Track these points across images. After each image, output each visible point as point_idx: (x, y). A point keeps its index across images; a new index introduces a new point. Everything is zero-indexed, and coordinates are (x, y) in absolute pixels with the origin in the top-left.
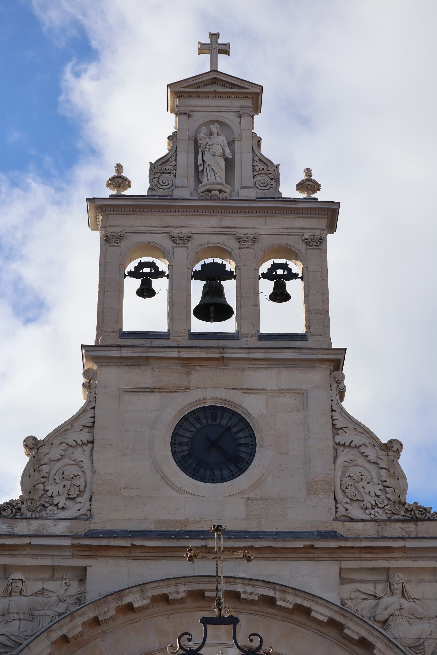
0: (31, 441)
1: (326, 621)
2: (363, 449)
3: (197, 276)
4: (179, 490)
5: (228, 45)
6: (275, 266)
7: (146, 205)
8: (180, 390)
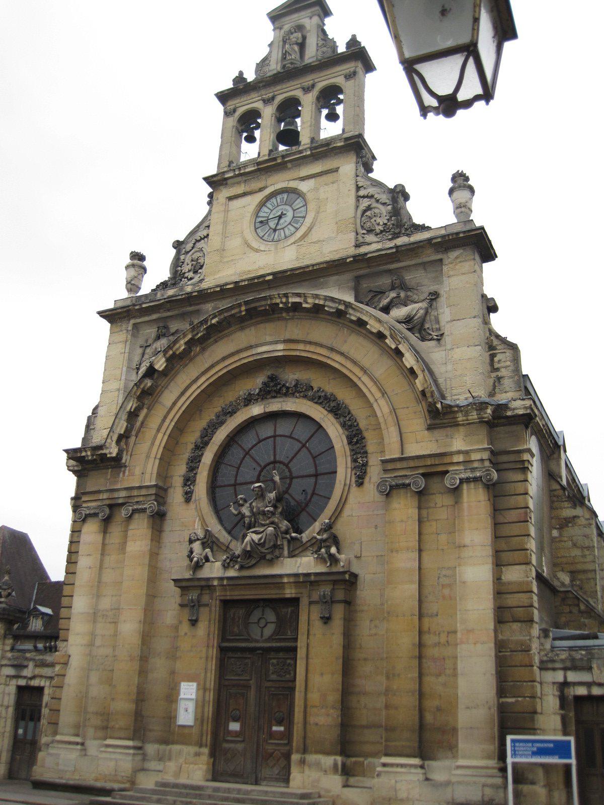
4: (257, 251)
8: (261, 190)
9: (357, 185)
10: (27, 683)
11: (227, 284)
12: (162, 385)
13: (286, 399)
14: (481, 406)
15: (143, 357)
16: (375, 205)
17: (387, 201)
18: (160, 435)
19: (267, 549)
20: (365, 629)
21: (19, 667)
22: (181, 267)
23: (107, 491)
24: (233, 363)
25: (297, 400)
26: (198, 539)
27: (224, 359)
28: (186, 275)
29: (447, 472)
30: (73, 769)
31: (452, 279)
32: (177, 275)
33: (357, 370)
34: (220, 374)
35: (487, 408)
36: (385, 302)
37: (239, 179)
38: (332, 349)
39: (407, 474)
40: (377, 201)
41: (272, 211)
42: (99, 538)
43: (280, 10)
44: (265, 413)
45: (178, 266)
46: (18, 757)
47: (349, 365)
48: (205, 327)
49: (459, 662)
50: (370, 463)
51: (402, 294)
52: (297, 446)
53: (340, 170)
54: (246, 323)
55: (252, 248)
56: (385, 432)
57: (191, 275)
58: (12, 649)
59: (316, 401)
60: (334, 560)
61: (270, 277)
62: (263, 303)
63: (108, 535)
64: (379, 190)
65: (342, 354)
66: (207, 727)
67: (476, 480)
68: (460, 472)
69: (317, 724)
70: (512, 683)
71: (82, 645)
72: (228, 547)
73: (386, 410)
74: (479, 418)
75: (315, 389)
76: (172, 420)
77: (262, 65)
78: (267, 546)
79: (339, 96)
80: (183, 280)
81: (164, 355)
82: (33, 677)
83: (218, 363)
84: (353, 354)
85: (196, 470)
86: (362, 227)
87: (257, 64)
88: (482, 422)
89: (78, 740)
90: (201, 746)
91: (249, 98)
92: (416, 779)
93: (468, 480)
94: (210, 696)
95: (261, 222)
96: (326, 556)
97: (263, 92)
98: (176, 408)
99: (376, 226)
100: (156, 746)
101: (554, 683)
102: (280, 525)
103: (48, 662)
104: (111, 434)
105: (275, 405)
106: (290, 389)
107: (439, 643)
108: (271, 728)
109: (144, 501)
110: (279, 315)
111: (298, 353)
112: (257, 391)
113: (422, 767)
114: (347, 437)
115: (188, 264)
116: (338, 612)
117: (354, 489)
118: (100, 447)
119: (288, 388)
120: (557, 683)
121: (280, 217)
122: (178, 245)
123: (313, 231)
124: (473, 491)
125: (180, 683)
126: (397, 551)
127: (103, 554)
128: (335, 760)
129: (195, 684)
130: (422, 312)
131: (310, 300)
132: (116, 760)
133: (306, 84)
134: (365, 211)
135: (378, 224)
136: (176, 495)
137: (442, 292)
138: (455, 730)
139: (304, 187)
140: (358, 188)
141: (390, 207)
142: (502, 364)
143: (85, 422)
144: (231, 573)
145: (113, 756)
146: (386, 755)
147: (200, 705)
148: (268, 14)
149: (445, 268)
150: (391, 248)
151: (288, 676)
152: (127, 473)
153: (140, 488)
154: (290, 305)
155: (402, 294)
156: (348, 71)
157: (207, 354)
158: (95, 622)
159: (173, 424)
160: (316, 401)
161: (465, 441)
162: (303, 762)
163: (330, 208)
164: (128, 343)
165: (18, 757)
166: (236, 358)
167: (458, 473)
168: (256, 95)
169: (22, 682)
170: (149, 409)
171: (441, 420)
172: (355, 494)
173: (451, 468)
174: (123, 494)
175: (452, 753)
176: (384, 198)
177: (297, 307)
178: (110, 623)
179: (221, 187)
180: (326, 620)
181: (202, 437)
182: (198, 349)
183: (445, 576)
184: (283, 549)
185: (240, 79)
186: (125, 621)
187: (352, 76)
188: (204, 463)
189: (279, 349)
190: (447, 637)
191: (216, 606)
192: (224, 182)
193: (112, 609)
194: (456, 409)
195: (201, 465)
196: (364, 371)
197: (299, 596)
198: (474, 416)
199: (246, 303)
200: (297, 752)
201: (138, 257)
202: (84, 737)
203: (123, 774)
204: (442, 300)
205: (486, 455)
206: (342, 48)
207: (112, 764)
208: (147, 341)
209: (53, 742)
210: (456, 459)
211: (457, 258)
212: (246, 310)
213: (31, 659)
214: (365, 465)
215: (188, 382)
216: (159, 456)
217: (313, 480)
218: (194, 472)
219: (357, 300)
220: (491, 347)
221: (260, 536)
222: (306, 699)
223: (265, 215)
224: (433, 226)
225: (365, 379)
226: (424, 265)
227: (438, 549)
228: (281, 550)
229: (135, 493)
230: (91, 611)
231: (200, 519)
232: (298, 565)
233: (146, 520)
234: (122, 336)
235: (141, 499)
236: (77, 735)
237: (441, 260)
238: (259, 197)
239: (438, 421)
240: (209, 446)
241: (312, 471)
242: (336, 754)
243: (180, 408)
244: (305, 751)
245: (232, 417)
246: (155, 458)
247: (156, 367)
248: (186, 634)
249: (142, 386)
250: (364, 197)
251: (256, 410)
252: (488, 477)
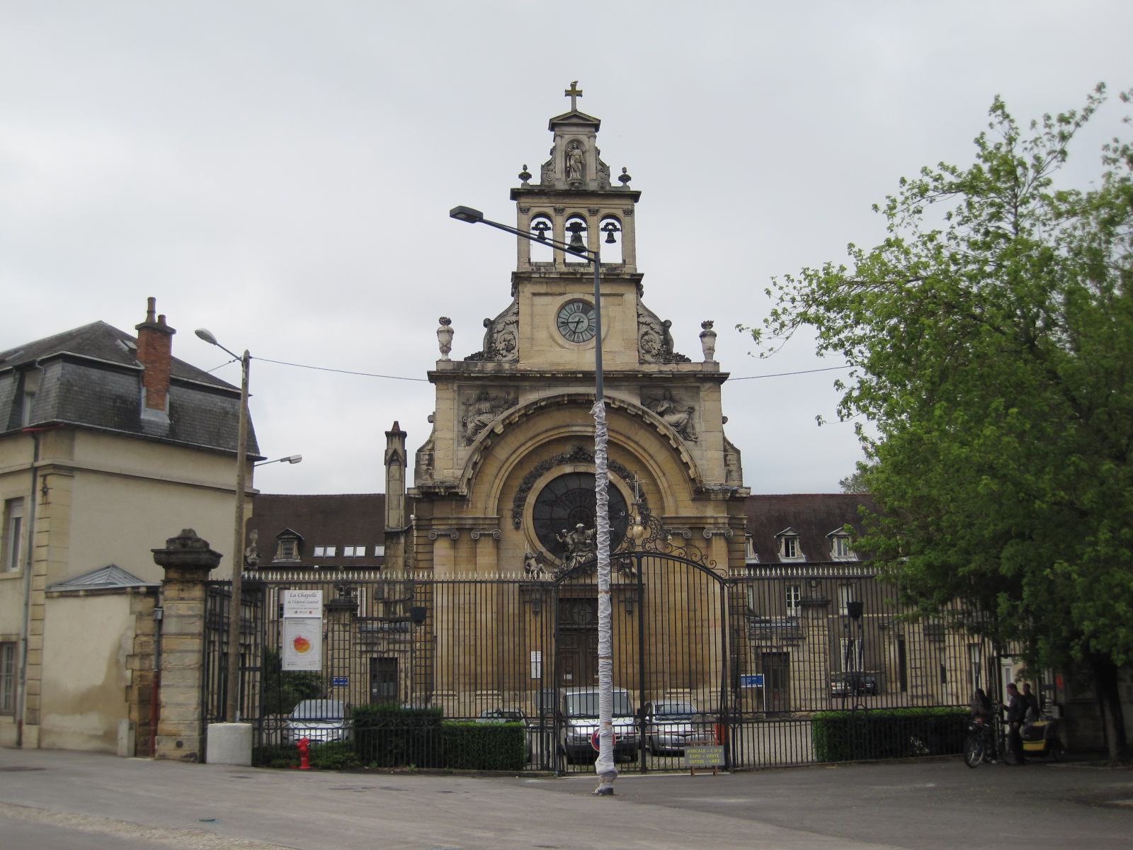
0: (487, 323)
2: (652, 325)
3: (568, 229)
4: (562, 347)
5: (581, 91)
6: (608, 224)
7: (97, 361)
8: (560, 294)
14: (725, 491)
16: (651, 332)
18: (497, 481)
20: (651, 617)
23: (455, 518)
24: (554, 435)
27: (546, 431)
28: (501, 352)
29: (704, 528)
31: (706, 403)
32: (490, 351)
33: (646, 455)
36: (660, 409)
38: (629, 438)
40: (652, 329)
53: (625, 296)
55: (559, 345)
56: (665, 499)
61: (581, 375)
62: (581, 398)
64: (653, 321)
68: (710, 529)
73: (666, 485)
83: (542, 433)
84: (641, 442)
88: (724, 500)
93: (716, 535)
95: (563, 323)
112: (568, 456)
121: (578, 323)
130: (686, 421)
131: (617, 403)
134: (643, 336)
136: (508, 524)
137: (697, 408)
140: (639, 315)
141: (662, 337)
142: (732, 462)
149: (701, 394)
152: (470, 506)
153: (485, 518)
156: (627, 207)
166: (556, 432)
167: (710, 531)
168: (547, 201)
173: (707, 526)
174: (470, 522)
176: (657, 328)
179: (526, 282)
198: (720, 496)
204: (696, 414)
205: (726, 521)
208: (468, 400)
210: (709, 521)
215: (518, 445)
219: (642, 404)
220: (725, 450)
223: (565, 317)
226: (686, 388)
229: (481, 522)
235: (486, 526)
237: (698, 387)
247: (496, 431)
251: (568, 469)
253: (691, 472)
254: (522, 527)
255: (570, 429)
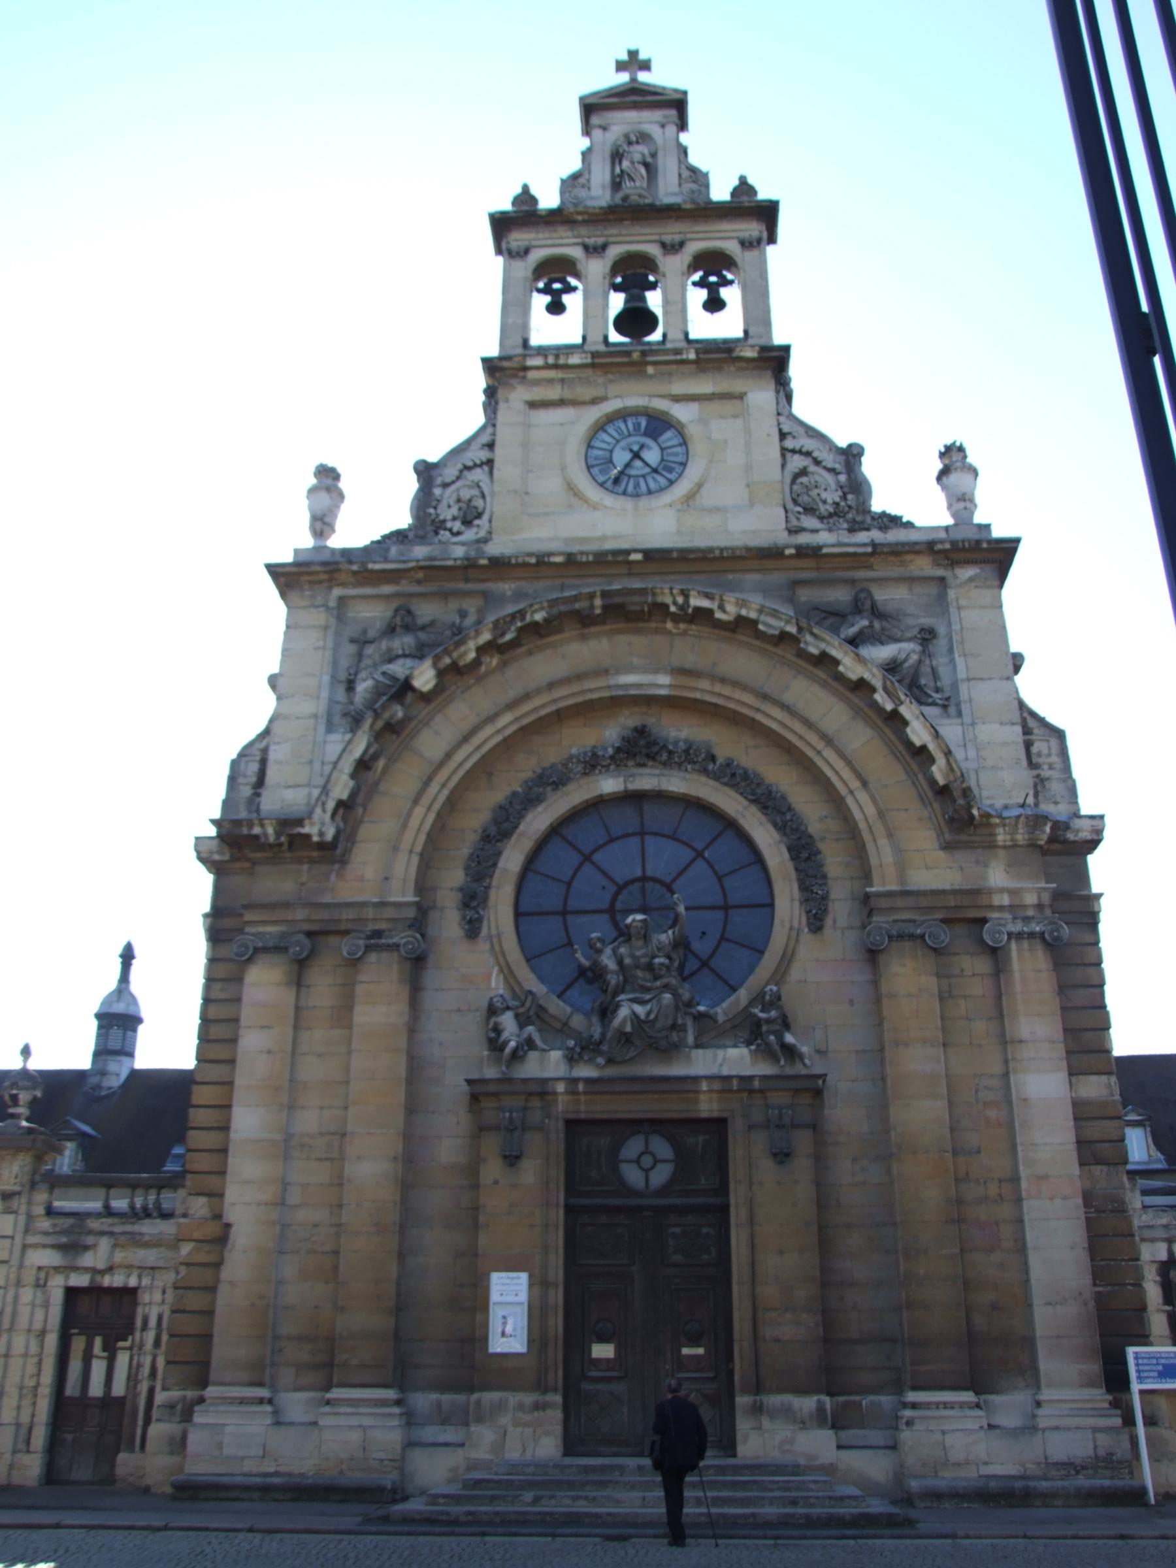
1: (498, 1345)
8: (595, 401)
9: (780, 430)
10: (92, 1280)
11: (550, 554)
12: (420, 717)
13: (666, 772)
15: (360, 661)
16: (812, 468)
17: (837, 466)
18: (419, 811)
19: (660, 1031)
21: (72, 1247)
22: (435, 508)
25: (688, 776)
26: (508, 1008)
28: (449, 525)
30: (260, 1453)
33: (813, 738)
34: (543, 712)
35: (1045, 824)
37: (552, 374)
38: (765, 697)
39: (917, 917)
41: (618, 441)
42: (288, 996)
43: (603, 98)
44: (626, 791)
45: (429, 506)
46: (69, 1437)
47: (797, 726)
48: (519, 624)
49: (1027, 1228)
50: (833, 896)
51: (877, 625)
52: (686, 854)
54: (593, 629)
57: (457, 526)
58: (50, 1212)
59: (725, 780)
60: (791, 1052)
62: (637, 598)
63: (304, 990)
65: (785, 707)
66: (556, 1355)
67: (1032, 935)
69: (778, 1340)
70: (1102, 1263)
71: (259, 1204)
72: (565, 1024)
74: (1029, 839)
75: (720, 760)
76: (444, 785)
77: (571, 183)
78: (659, 1025)
79: (725, 273)
80: (442, 532)
81: (435, 665)
82: (110, 1269)
85: (488, 880)
86: (795, 502)
87: (563, 182)
88: (1033, 845)
89: (264, 1393)
90: (545, 1391)
91: (554, 235)
92: (976, 1427)
93: (1019, 936)
94: (557, 1296)
96: (777, 1048)
97: (583, 231)
98: (452, 765)
99: (821, 504)
100: (434, 1396)
101: (1153, 1262)
102: (681, 991)
103: (147, 1238)
104: (323, 798)
105: (647, 780)
106: (676, 755)
107: (986, 1198)
108: (680, 1351)
109: (390, 930)
110: (660, 625)
111: (698, 696)
112: (610, 751)
113: (398, 1403)
114: (789, 849)
115: (449, 506)
116: (803, 1141)
117: (806, 936)
118: (300, 822)
119: (670, 753)
120: (1156, 1262)
122: (425, 471)
123: (704, 491)
124: (1027, 954)
125: (488, 1275)
126: (906, 1045)
127: (296, 1028)
128: (819, 1401)
129: (524, 1276)
132: (364, 1429)
133: (667, 239)
134: (796, 476)
135: (825, 502)
138: (1029, 1342)
139: (682, 413)
140: (783, 436)
143: (226, 771)
144: (585, 1071)
145: (354, 1421)
146: (915, 1388)
147: (537, 1313)
148: (582, 99)
150: (865, 545)
151: (705, 1257)
154: (690, 611)
155: (877, 625)
157: (510, 672)
158: (286, 1157)
159: (446, 792)
160: (725, 780)
161: (1008, 873)
162: (757, 1410)
163: (734, 458)
164: (331, 631)
165: (69, 1437)
169: (80, 1280)
170: (392, 760)
171: (970, 835)
172: (809, 950)
175: (1025, 1380)
177: (703, 615)
178: (320, 1159)
179: (514, 381)
180: (782, 1156)
181: (496, 821)
182: (495, 662)
183: (986, 1088)
184: (686, 1031)
185: (525, 198)
186: (359, 1157)
187: (755, 244)
188: (505, 870)
189: (662, 683)
190: (1000, 1187)
191: (557, 1129)
192: (521, 374)
193: (321, 1134)
194: (997, 821)
195: (498, 872)
196: (829, 741)
197: (725, 1115)
199: (605, 594)
200: (744, 1391)
201: (327, 477)
202: (273, 1387)
203: (381, 1455)
206: (720, 192)
207: (355, 1437)
209: (201, 1400)
211: (971, 579)
212: (604, 607)
213: (103, 1233)
214: (825, 898)
216: (418, 848)
217: (720, 914)
218: (485, 884)
220: (1027, 731)
221: (648, 1007)
222: (754, 1297)
224: (918, 523)
225: (829, 754)
227: (971, 1044)
228: (681, 1034)
230: (279, 1137)
231: (501, 971)
232: (719, 1061)
233: (395, 967)
234: (318, 617)
236: (260, 1384)
238: (594, 414)
239: (963, 837)
240: (514, 838)
241: (718, 899)
242: (818, 1391)
243: (460, 765)
244: (758, 1388)
245: (559, 793)
246: (411, 852)
248: (496, 1182)
249: (386, 715)
250: (793, 451)
251: (610, 785)
252: (1055, 934)
253: (938, 771)
254: (484, 932)
255: (612, 681)
